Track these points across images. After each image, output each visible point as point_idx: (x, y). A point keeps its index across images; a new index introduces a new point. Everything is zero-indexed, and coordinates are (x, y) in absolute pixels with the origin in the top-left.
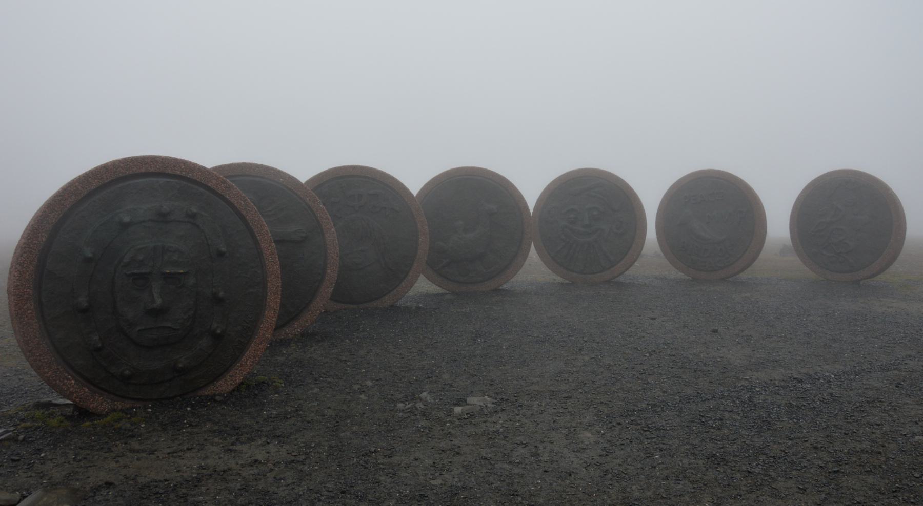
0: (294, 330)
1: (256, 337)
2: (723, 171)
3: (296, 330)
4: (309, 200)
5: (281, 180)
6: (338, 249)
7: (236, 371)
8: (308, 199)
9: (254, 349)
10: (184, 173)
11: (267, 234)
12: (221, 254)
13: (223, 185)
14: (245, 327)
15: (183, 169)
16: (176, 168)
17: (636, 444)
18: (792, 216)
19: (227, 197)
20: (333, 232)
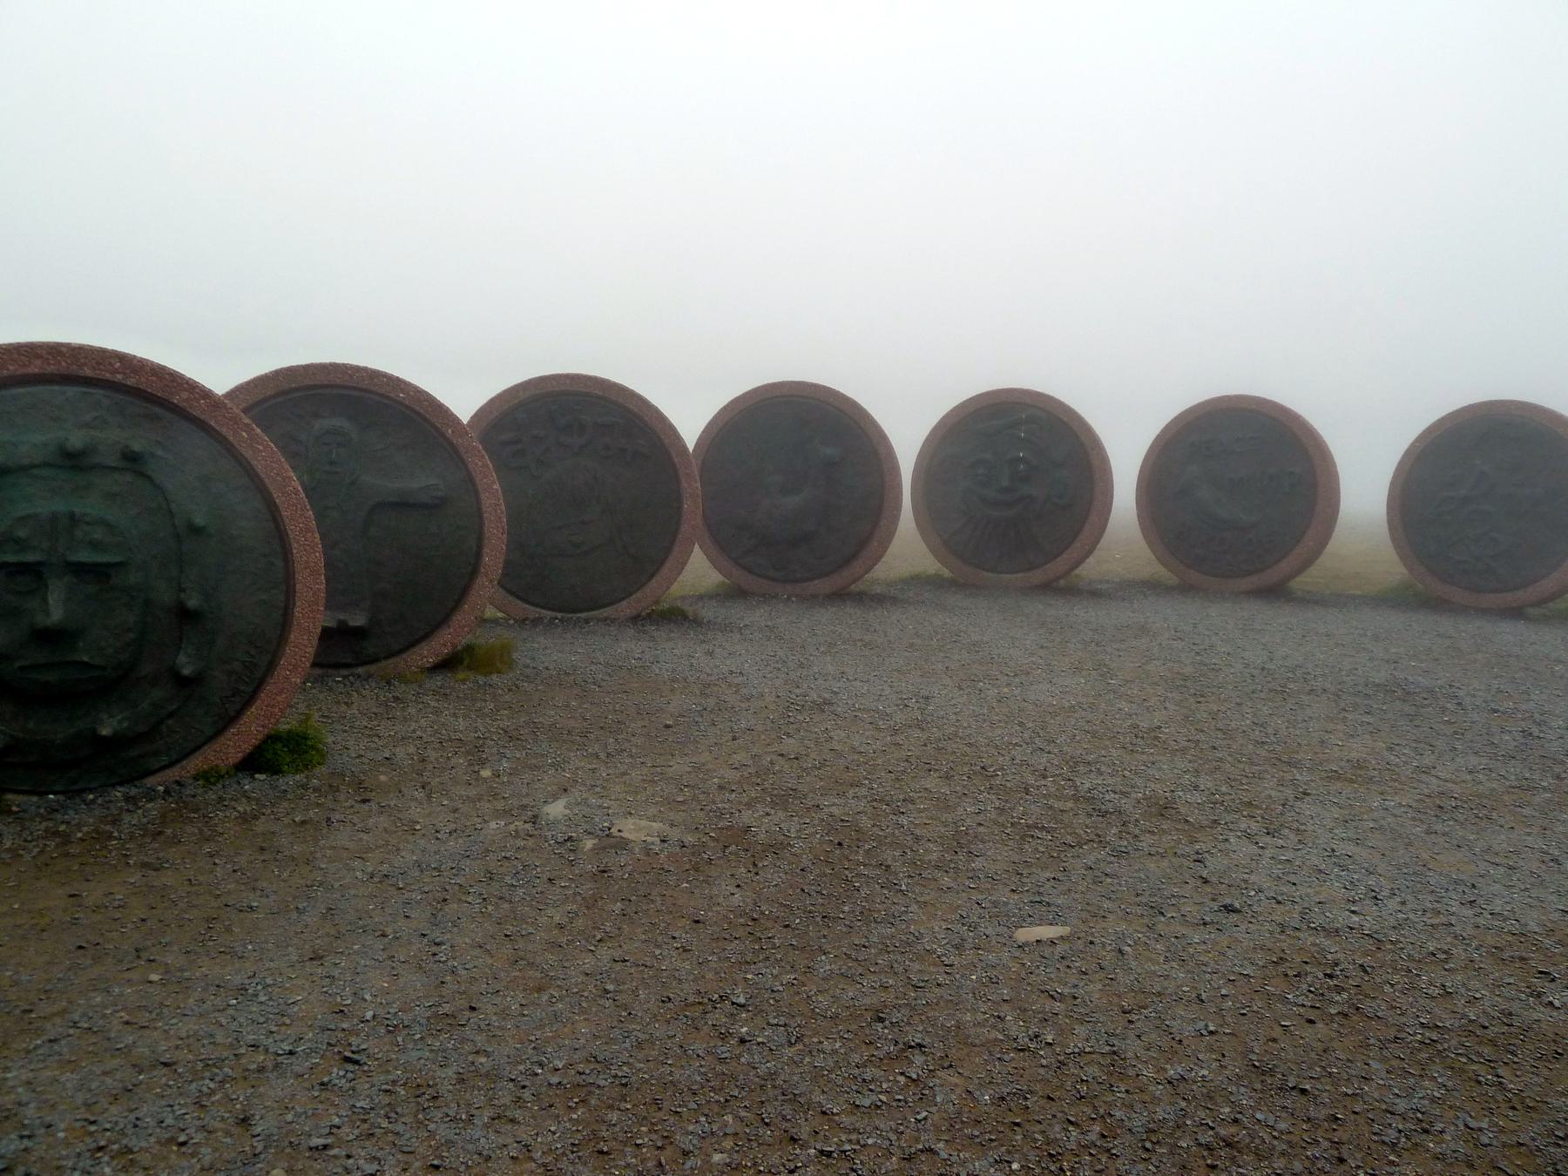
0: (422, 660)
1: (272, 681)
2: (1190, 408)
3: (425, 660)
4: (453, 432)
5: (401, 395)
6: (505, 520)
7: (228, 742)
8: (450, 431)
9: (266, 703)
10: (119, 377)
11: (296, 494)
12: (195, 530)
13: (202, 401)
14: (247, 664)
15: (117, 369)
16: (101, 367)
17: (1379, 671)
18: (1393, 484)
19: (213, 423)
20: (497, 490)
